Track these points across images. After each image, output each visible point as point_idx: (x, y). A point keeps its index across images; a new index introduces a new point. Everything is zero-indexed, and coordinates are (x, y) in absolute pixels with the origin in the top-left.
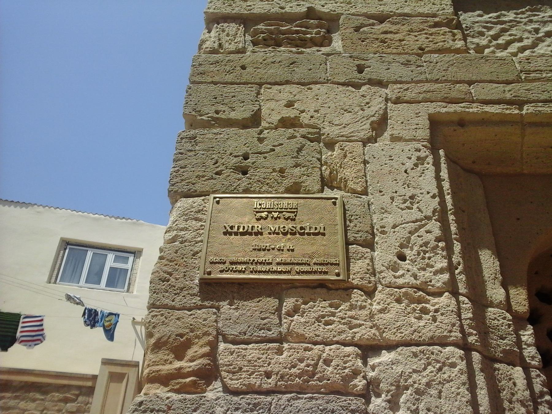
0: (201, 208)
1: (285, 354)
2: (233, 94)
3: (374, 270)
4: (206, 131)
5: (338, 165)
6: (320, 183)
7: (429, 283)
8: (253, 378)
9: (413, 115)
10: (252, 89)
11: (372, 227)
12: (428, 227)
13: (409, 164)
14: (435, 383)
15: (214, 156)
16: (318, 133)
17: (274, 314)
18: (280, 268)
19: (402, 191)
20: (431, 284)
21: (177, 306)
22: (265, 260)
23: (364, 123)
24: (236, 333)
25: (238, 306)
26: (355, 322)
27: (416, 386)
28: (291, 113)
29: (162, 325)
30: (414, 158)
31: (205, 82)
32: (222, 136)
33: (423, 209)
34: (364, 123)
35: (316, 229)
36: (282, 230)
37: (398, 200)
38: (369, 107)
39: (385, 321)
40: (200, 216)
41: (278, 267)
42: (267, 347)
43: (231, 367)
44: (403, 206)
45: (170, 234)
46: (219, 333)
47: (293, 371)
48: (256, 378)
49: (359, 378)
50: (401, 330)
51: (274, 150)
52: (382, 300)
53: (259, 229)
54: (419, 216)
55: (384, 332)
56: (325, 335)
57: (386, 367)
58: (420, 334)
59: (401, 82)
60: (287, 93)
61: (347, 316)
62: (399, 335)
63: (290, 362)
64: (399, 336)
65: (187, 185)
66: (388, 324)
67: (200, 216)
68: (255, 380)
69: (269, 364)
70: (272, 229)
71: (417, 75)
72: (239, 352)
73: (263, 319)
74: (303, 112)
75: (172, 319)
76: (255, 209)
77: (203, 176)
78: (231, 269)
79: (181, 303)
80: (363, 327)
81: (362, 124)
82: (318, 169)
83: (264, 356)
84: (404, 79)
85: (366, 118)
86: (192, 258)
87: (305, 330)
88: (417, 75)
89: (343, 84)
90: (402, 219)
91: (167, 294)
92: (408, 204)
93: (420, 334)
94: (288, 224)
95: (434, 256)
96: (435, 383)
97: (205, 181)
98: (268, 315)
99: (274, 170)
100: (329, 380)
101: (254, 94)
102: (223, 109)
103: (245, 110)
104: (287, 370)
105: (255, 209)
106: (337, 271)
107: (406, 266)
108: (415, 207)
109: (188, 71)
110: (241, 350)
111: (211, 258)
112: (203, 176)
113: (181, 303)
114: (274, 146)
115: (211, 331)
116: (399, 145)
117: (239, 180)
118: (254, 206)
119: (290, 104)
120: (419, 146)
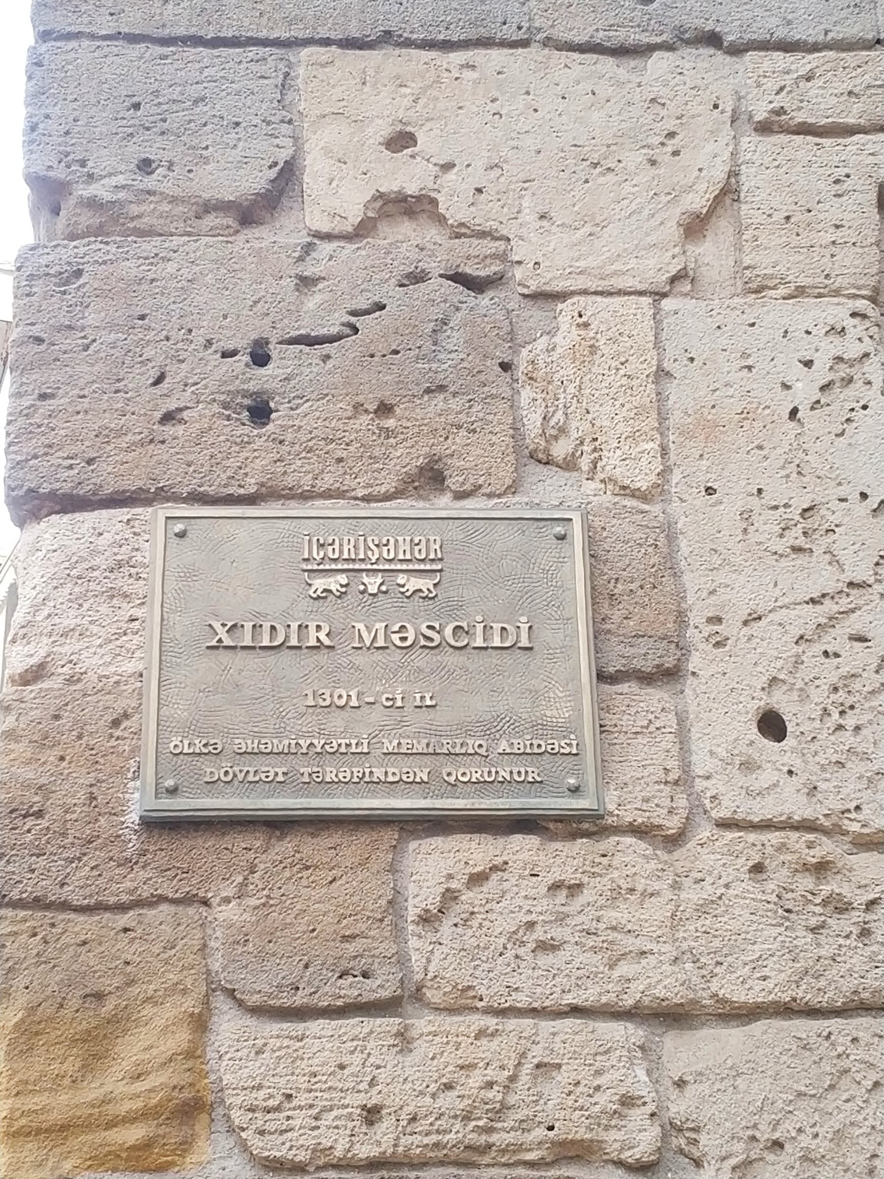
0: (124, 553)
1: (422, 1048)
2: (194, 91)
3: (686, 766)
4: (112, 248)
5: (571, 389)
6: (511, 458)
7: (853, 815)
8: (328, 1127)
9: (825, 187)
10: (262, 69)
11: (681, 618)
12: (855, 624)
13: (805, 390)
14: (858, 1132)
15: (149, 353)
16: (502, 257)
17: (381, 920)
18: (394, 772)
19: (777, 492)
20: (860, 817)
21: (77, 900)
22: (348, 745)
23: (658, 218)
24: (267, 989)
25: (268, 897)
26: (631, 943)
27: (805, 1140)
28: (408, 176)
29: (38, 964)
30: (822, 362)
31: (93, 37)
32: (171, 267)
33: (846, 557)
34: (658, 218)
35: (539, 746)
36: (395, 638)
37: (766, 525)
38: (676, 153)
39: (717, 943)
40: (121, 582)
41: (391, 770)
42: (366, 1030)
43: (262, 1094)
44: (781, 546)
45: (30, 649)
46: (213, 987)
47: (447, 1101)
48: (337, 1127)
49: (638, 1115)
50: (766, 972)
51: (356, 330)
52: (710, 873)
53: (322, 636)
54: (826, 579)
55: (714, 975)
56: (539, 990)
57: (717, 1086)
58: (822, 983)
59: (788, 47)
60: (384, 87)
61: (602, 926)
62: (758, 985)
63: (435, 1076)
64: (757, 988)
65: (71, 467)
66: (725, 951)
67: (121, 582)
68: (333, 1134)
69: (372, 1083)
70: (365, 634)
71: (843, 14)
72: (280, 1049)
73: (346, 939)
74: (448, 167)
75: (68, 946)
76: (306, 560)
77: (121, 433)
78: (241, 777)
79: (87, 891)
80: (652, 960)
81: (653, 223)
82: (503, 406)
83: (358, 1058)
84: (798, 34)
85: (664, 199)
86: (111, 736)
87: (477, 973)
88: (843, 14)
89: (582, 48)
90: (778, 592)
91: (42, 862)
92: (795, 536)
93: (822, 983)
94: (415, 616)
95: (870, 722)
96: (858, 1132)
97: (127, 450)
98: (362, 926)
99: (358, 408)
100: (551, 1128)
101: (269, 89)
102: (167, 156)
103: (245, 161)
104: (428, 1100)
105: (306, 560)
106: (572, 781)
107: (785, 759)
108: (820, 544)
109: (31, 25)
110: (286, 1042)
111: (176, 741)
112: (121, 433)
113: (87, 891)
114: (354, 313)
115: (189, 982)
116: (775, 313)
117: (243, 444)
118: (300, 551)
119: (401, 141)
120: (837, 311)
